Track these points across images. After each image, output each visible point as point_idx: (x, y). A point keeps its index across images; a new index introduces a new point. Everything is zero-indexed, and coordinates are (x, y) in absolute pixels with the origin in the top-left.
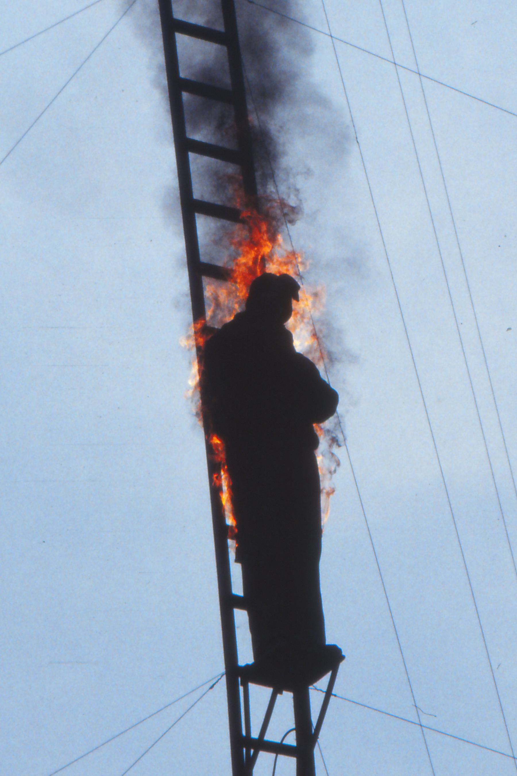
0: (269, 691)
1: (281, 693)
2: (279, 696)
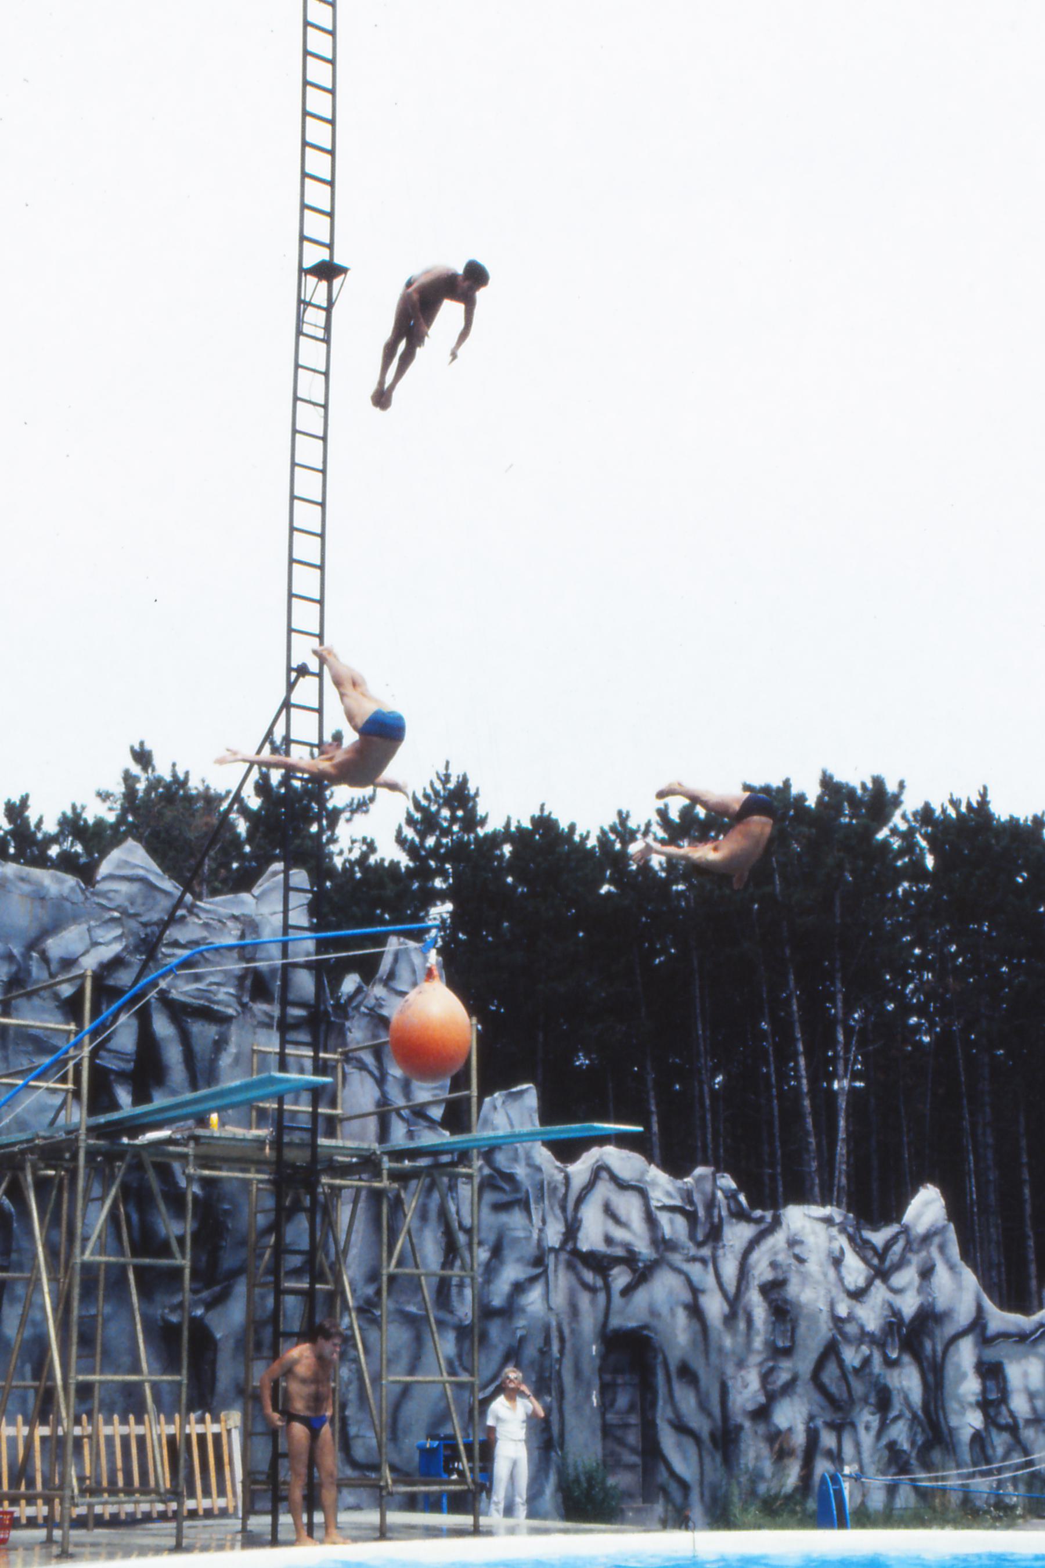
0: (315, 280)
1: (303, 676)
2: (301, 679)
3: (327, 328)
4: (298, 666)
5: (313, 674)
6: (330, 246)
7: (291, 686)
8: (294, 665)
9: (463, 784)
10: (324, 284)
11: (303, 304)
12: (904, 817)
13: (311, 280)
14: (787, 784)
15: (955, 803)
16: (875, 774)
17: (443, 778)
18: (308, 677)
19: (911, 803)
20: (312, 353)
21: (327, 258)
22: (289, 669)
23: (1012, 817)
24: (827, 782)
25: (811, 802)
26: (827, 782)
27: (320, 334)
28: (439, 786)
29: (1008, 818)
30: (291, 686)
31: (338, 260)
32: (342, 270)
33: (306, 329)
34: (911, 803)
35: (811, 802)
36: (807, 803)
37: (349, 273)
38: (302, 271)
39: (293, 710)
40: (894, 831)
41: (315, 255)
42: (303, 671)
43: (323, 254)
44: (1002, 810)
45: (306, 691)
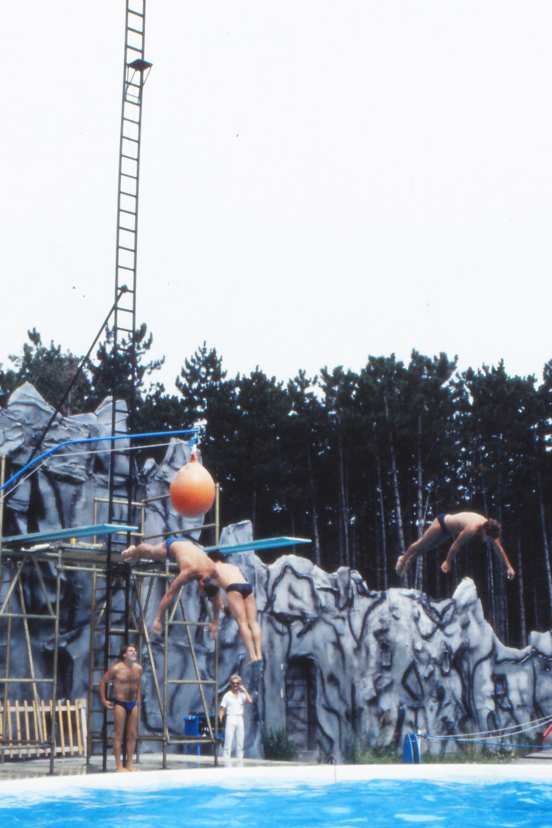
0: (133, 70)
3: (140, 97)
4: (122, 287)
5: (130, 291)
6: (142, 52)
7: (117, 298)
8: (119, 286)
9: (213, 354)
10: (139, 73)
11: (126, 84)
12: (457, 375)
13: (131, 70)
14: (393, 356)
15: (485, 368)
16: (442, 352)
17: (202, 351)
18: (127, 293)
19: (461, 368)
20: (132, 112)
21: (140, 58)
22: (117, 288)
23: (516, 377)
24: (415, 356)
25: (406, 366)
26: (415, 356)
27: (136, 101)
28: (200, 355)
29: (514, 377)
30: (117, 298)
31: (146, 59)
32: (148, 65)
33: (128, 98)
34: (461, 368)
35: (406, 366)
36: (404, 367)
37: (152, 67)
38: (126, 65)
39: (118, 311)
40: (452, 383)
41: (133, 56)
42: (124, 289)
43: (138, 56)
44: (511, 373)
45: (126, 301)
